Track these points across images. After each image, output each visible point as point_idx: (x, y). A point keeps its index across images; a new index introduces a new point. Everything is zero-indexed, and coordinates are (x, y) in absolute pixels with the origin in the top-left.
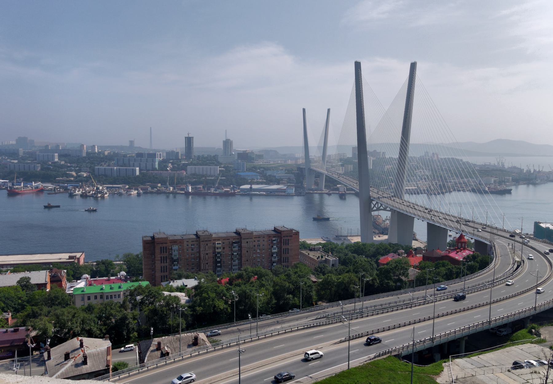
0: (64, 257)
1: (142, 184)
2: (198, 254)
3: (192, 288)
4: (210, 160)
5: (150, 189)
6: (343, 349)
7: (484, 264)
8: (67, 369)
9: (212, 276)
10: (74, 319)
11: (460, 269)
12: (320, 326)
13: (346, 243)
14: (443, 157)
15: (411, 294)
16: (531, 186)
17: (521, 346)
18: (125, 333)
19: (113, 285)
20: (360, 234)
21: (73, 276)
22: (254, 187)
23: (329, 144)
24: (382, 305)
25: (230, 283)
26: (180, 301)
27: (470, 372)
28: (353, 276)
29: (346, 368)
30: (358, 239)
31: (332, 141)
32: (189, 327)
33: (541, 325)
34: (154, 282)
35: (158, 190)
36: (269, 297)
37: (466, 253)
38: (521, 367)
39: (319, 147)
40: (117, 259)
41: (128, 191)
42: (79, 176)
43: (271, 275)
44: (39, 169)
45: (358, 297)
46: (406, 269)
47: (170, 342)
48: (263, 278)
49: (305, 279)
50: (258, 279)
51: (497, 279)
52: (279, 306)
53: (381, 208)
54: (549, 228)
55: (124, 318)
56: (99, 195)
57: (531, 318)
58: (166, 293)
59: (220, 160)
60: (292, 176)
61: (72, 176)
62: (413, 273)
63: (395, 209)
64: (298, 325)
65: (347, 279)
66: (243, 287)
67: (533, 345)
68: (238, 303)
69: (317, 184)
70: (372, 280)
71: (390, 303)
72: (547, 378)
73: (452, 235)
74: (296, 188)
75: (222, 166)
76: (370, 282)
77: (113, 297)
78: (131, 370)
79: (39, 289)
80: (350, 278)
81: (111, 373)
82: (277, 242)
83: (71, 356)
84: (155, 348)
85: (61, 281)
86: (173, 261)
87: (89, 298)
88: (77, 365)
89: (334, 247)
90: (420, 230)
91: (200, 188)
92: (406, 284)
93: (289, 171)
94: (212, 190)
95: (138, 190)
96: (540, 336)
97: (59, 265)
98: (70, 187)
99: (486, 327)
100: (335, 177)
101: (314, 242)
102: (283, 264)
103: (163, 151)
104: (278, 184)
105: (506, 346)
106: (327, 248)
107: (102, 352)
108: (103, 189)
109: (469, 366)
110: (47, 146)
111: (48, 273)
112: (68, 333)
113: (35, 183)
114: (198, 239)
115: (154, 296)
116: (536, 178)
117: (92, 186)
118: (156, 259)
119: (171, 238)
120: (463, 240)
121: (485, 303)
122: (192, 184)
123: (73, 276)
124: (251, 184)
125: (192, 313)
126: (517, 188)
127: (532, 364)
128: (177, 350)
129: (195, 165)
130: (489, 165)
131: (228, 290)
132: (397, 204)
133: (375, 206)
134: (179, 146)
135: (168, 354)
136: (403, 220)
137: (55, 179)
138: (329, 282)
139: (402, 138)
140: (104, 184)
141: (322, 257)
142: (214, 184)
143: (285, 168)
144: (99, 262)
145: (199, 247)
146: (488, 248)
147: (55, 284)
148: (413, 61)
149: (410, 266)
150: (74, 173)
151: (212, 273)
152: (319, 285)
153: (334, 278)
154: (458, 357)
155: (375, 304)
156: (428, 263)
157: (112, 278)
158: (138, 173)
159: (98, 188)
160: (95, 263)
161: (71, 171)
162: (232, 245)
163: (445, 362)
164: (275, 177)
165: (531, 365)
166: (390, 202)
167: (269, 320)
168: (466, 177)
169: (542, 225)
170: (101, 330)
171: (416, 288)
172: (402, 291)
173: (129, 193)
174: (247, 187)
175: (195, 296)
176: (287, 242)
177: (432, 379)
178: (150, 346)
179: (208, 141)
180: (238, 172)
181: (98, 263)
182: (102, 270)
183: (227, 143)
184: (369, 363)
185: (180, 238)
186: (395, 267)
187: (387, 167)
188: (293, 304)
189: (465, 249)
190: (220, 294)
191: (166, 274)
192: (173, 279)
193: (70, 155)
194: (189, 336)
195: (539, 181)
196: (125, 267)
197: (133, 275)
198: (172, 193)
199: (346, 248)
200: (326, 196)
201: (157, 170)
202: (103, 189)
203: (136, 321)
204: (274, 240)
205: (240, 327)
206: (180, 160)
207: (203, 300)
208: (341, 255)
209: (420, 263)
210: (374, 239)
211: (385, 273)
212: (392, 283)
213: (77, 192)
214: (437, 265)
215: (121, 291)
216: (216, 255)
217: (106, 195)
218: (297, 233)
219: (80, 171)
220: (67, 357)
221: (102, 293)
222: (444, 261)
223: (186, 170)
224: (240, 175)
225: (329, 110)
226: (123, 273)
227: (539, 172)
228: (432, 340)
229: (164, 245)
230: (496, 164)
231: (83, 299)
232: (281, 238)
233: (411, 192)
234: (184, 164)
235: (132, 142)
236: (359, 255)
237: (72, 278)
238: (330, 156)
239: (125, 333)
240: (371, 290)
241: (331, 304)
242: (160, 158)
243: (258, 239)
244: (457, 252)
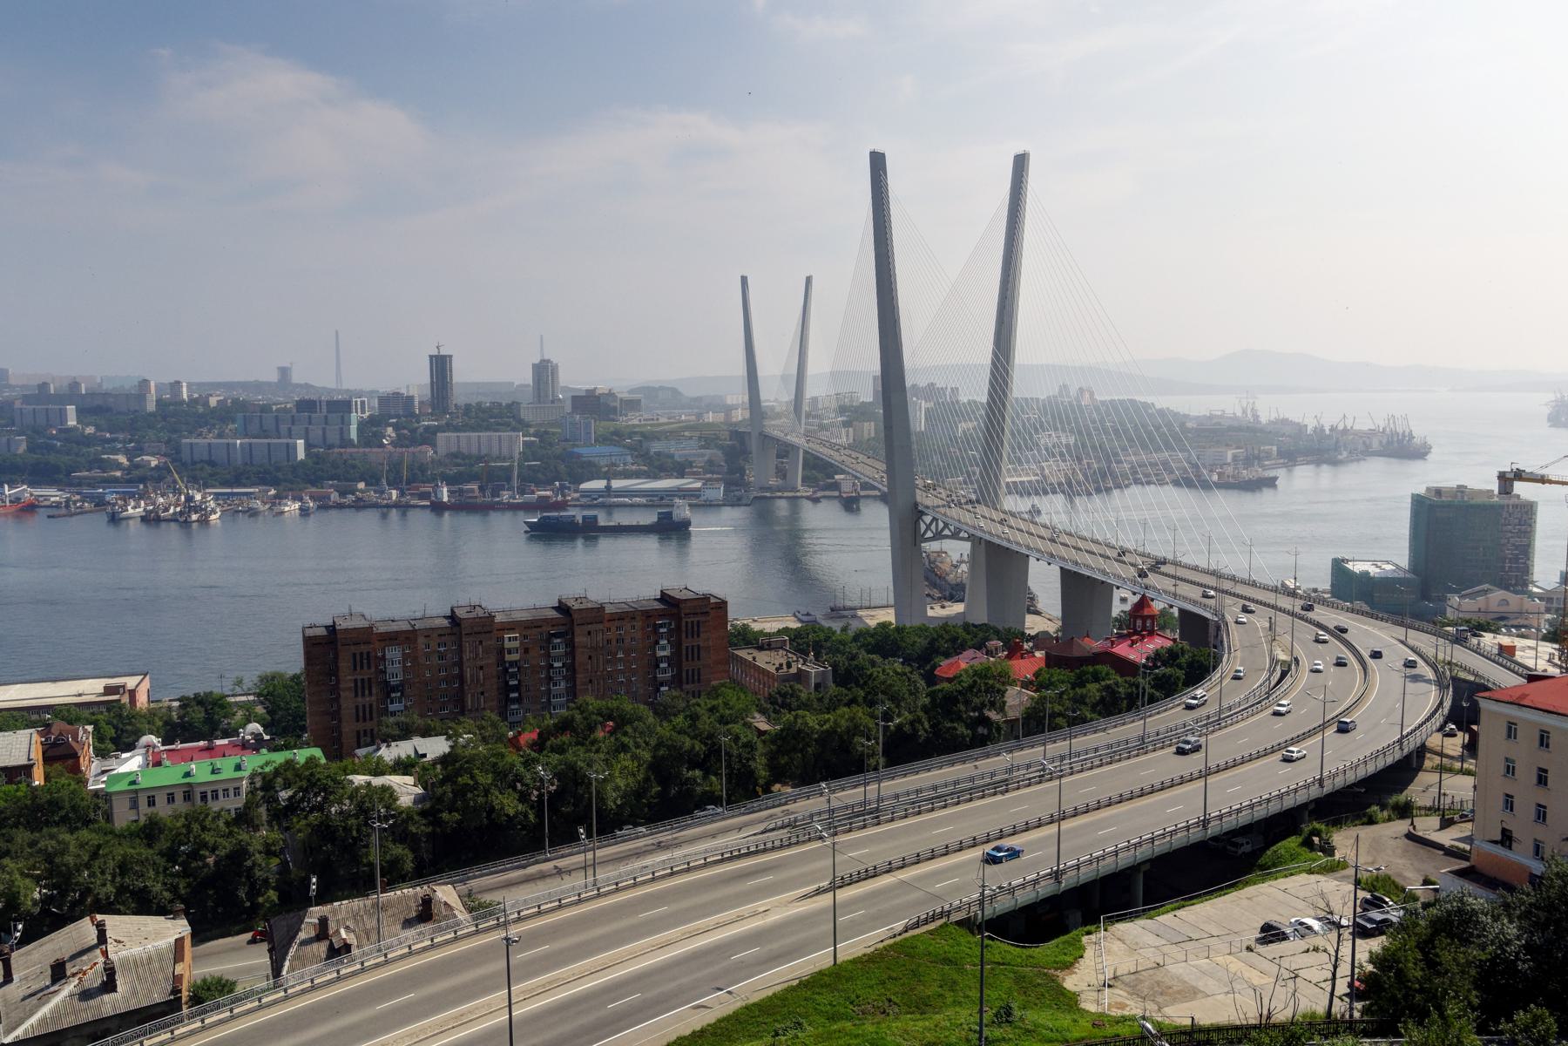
0: (91, 688)
1: (313, 484)
2: (459, 664)
3: (435, 762)
4: (495, 414)
5: (335, 496)
6: (821, 912)
7: (1198, 672)
8: (57, 1006)
9: (494, 725)
10: (97, 863)
11: (1137, 687)
12: (765, 851)
13: (855, 625)
14: (1108, 398)
15: (1008, 757)
16: (1325, 467)
17: (1282, 883)
18: (242, 894)
19: (219, 762)
20: (892, 602)
21: (115, 741)
22: (617, 484)
23: (812, 369)
24: (935, 788)
25: (539, 746)
26: (397, 799)
27: (1149, 957)
28: (860, 712)
29: (827, 963)
30: (888, 616)
31: (817, 365)
32: (426, 870)
33: (1337, 823)
34: (337, 750)
35: (359, 499)
36: (640, 777)
37: (1153, 645)
38: (1282, 937)
39: (784, 378)
40: (238, 690)
41: (274, 504)
42: (137, 466)
43: (651, 720)
44: (23, 448)
45: (876, 769)
46: (999, 691)
47: (355, 916)
48: (629, 729)
49: (736, 728)
50: (612, 733)
51: (1230, 709)
52: (667, 799)
53: (946, 532)
54: (1367, 573)
55: (240, 854)
56: (194, 517)
57: (1312, 807)
58: (359, 779)
59: (525, 415)
61: (119, 466)
62: (1017, 699)
63: (979, 534)
64: (706, 851)
65: (843, 723)
66: (570, 756)
67: (1314, 878)
68: (555, 798)
69: (782, 473)
70: (912, 723)
71: (956, 783)
72: (1335, 967)
73: (1121, 603)
74: (729, 484)
75: (532, 430)
76: (907, 728)
77: (221, 794)
78: (238, 1000)
79: (10, 782)
80: (852, 719)
81: (185, 1011)
82: (670, 630)
83: (70, 970)
84: (313, 934)
85: (75, 756)
86: (388, 690)
87: (151, 802)
88: (86, 995)
89: (822, 636)
90: (1044, 583)
91: (472, 491)
92: (999, 729)
93: (707, 437)
94: (505, 496)
95: (301, 500)
96: (1332, 854)
97: (70, 714)
98: (109, 498)
99: (1196, 835)
100: (825, 452)
101: (771, 626)
102: (685, 686)
103: (371, 394)
104: (681, 475)
105: (1247, 884)
106: (804, 641)
107: (160, 954)
108: (203, 501)
109: (1150, 939)
110: (44, 385)
111: (36, 737)
112: (82, 900)
113: (11, 488)
114: (456, 630)
115: (325, 789)
116: (1336, 449)
117: (174, 493)
118: (342, 686)
119: (382, 629)
120: (1146, 612)
121: (1238, 757)
122: (450, 481)
123: (113, 740)
124: (608, 477)
125: (430, 829)
127: (1309, 928)
128: (374, 937)
129: (457, 429)
130: (1221, 417)
131: (528, 763)
132: (984, 521)
133: (928, 527)
134: (415, 381)
135: (347, 948)
136: (1001, 564)
137: (68, 474)
138: (799, 731)
139: (994, 353)
140: (206, 486)
141: (789, 666)
142: (509, 479)
143: (697, 434)
144: (188, 698)
145: (460, 650)
146: (1212, 631)
147: (58, 766)
149: (1013, 683)
150: (122, 459)
151: (495, 717)
152: (773, 742)
153: (812, 720)
154: (1120, 919)
155: (917, 786)
156: (1058, 674)
157: (218, 742)
158: (301, 455)
159: (190, 499)
160: (176, 704)
161: (116, 452)
162: (549, 641)
163: (1089, 933)
164: (672, 456)
165: (1304, 930)
166: (967, 518)
167: (643, 838)
168: (1169, 447)
169: (1350, 566)
170: (174, 889)
171: (1025, 741)
172: (990, 748)
173: (276, 509)
174: (599, 484)
175: (442, 782)
176: (695, 630)
177: (1053, 979)
178: (299, 930)
179: (490, 366)
180: (574, 446)
181: (1428, 489)
182: (197, 722)
183: (544, 372)
184: (891, 946)
185: (405, 627)
186: (971, 687)
187: (962, 426)
188: (705, 793)
189: (1151, 633)
190: (506, 776)
191: (369, 725)
192: (388, 739)
193: (109, 410)
194: (409, 894)
195: (1345, 454)
196: (260, 710)
197: (284, 732)
198: (396, 505)
199: (856, 638)
200: (807, 504)
201: (354, 446)
202: (203, 501)
203: (275, 862)
204: (661, 626)
205: (561, 863)
206: (418, 418)
207: (461, 792)
208: (839, 658)
209: (1037, 675)
210: (930, 613)
211: (945, 705)
212: (961, 729)
213: (131, 511)
214: (1079, 677)
215: (241, 779)
216: (506, 670)
217: (213, 517)
218: (722, 605)
219: (140, 450)
220: (58, 972)
221: (189, 784)
222: (1098, 667)
223: (434, 445)
224: (579, 456)
225: (809, 280)
227: (1345, 431)
228: (1057, 875)
229: (364, 648)
230: (1239, 414)
231: (134, 805)
232: (680, 619)
233: (1016, 489)
234: (427, 428)
235: (284, 372)
236: (885, 657)
237: (111, 746)
238: (815, 400)
239: (242, 894)
240: (905, 750)
241: (805, 789)
242: (363, 412)
243: (617, 623)
244: (1134, 642)
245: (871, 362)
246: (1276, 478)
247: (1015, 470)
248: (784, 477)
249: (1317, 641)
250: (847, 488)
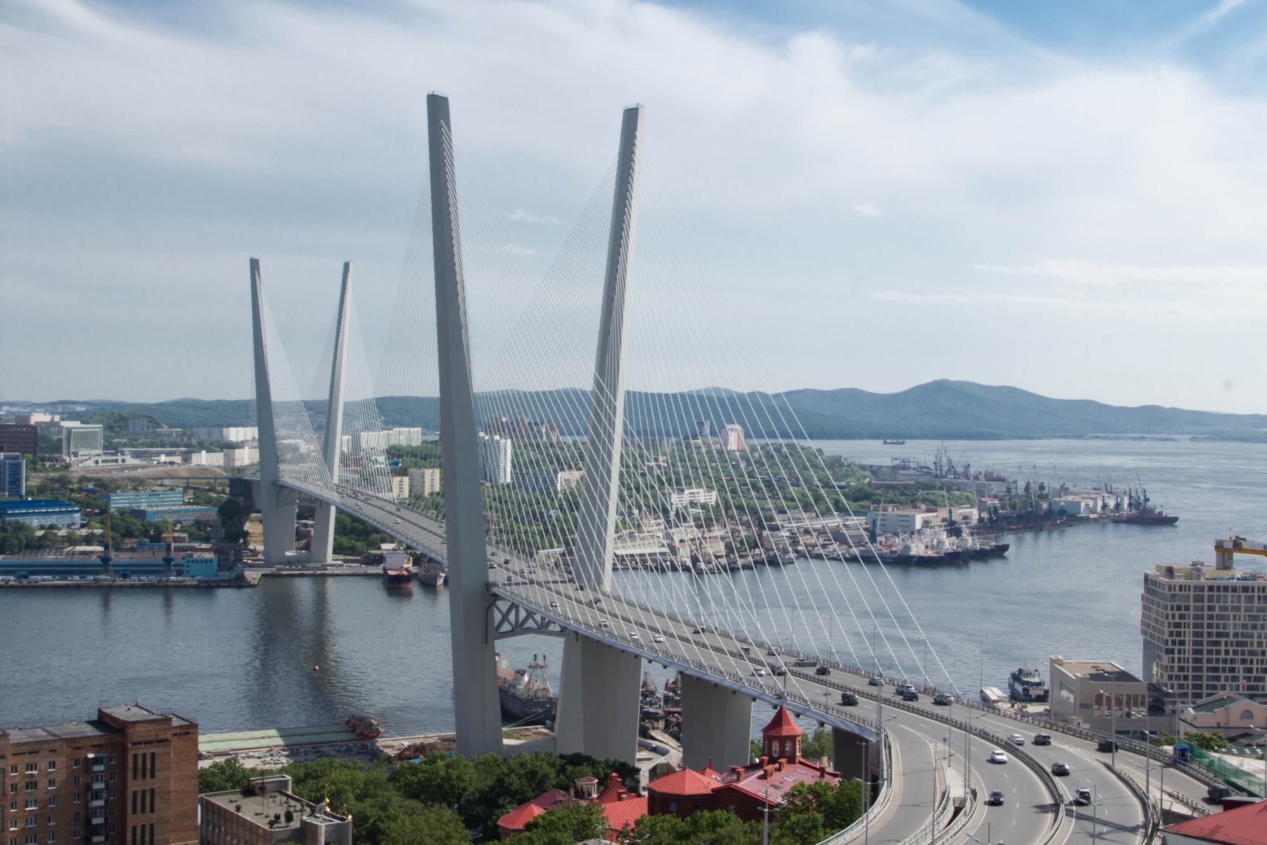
53: (530, 623)
82: (109, 768)
100: (371, 514)
126: (1020, 540)
132: (571, 608)
133: (505, 617)
141: (289, 818)
148: (632, 105)
176: (148, 768)
225: (631, 117)
226: (1169, 749)
232: (124, 751)
243: (28, 759)
245: (327, 397)
247: (631, 535)
248: (307, 547)
249: (993, 761)
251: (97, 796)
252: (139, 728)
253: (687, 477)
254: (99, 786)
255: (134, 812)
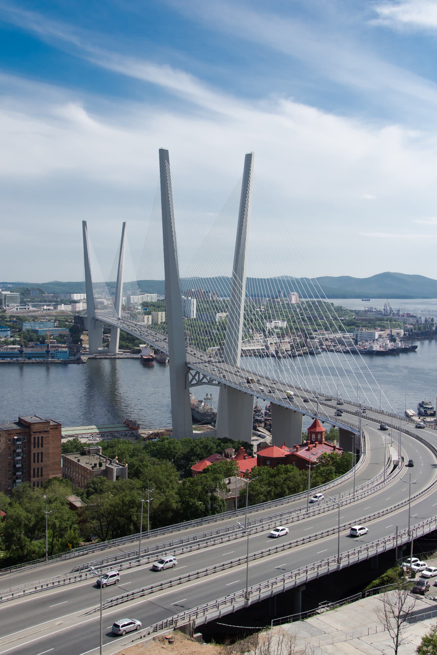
7: (343, 467)
53: (205, 380)
60: (66, 331)
62: (237, 484)
82: (23, 443)
120: (318, 430)
126: (422, 344)
133: (194, 378)
141: (101, 465)
176: (40, 443)
232: (30, 435)
240: (164, 519)
246: (416, 347)
248: (108, 346)
250: (148, 353)
251: (18, 455)
252: (36, 426)
253: (273, 315)
254: (19, 450)
255: (34, 462)
